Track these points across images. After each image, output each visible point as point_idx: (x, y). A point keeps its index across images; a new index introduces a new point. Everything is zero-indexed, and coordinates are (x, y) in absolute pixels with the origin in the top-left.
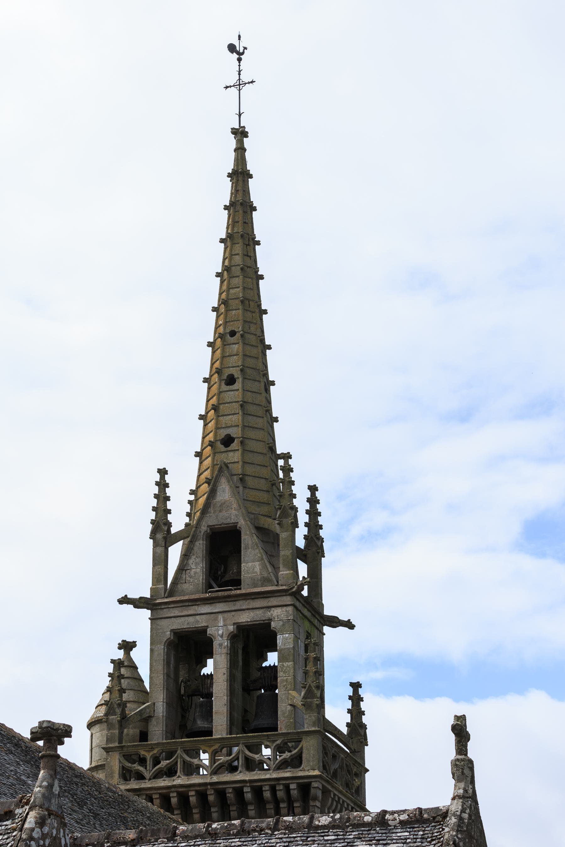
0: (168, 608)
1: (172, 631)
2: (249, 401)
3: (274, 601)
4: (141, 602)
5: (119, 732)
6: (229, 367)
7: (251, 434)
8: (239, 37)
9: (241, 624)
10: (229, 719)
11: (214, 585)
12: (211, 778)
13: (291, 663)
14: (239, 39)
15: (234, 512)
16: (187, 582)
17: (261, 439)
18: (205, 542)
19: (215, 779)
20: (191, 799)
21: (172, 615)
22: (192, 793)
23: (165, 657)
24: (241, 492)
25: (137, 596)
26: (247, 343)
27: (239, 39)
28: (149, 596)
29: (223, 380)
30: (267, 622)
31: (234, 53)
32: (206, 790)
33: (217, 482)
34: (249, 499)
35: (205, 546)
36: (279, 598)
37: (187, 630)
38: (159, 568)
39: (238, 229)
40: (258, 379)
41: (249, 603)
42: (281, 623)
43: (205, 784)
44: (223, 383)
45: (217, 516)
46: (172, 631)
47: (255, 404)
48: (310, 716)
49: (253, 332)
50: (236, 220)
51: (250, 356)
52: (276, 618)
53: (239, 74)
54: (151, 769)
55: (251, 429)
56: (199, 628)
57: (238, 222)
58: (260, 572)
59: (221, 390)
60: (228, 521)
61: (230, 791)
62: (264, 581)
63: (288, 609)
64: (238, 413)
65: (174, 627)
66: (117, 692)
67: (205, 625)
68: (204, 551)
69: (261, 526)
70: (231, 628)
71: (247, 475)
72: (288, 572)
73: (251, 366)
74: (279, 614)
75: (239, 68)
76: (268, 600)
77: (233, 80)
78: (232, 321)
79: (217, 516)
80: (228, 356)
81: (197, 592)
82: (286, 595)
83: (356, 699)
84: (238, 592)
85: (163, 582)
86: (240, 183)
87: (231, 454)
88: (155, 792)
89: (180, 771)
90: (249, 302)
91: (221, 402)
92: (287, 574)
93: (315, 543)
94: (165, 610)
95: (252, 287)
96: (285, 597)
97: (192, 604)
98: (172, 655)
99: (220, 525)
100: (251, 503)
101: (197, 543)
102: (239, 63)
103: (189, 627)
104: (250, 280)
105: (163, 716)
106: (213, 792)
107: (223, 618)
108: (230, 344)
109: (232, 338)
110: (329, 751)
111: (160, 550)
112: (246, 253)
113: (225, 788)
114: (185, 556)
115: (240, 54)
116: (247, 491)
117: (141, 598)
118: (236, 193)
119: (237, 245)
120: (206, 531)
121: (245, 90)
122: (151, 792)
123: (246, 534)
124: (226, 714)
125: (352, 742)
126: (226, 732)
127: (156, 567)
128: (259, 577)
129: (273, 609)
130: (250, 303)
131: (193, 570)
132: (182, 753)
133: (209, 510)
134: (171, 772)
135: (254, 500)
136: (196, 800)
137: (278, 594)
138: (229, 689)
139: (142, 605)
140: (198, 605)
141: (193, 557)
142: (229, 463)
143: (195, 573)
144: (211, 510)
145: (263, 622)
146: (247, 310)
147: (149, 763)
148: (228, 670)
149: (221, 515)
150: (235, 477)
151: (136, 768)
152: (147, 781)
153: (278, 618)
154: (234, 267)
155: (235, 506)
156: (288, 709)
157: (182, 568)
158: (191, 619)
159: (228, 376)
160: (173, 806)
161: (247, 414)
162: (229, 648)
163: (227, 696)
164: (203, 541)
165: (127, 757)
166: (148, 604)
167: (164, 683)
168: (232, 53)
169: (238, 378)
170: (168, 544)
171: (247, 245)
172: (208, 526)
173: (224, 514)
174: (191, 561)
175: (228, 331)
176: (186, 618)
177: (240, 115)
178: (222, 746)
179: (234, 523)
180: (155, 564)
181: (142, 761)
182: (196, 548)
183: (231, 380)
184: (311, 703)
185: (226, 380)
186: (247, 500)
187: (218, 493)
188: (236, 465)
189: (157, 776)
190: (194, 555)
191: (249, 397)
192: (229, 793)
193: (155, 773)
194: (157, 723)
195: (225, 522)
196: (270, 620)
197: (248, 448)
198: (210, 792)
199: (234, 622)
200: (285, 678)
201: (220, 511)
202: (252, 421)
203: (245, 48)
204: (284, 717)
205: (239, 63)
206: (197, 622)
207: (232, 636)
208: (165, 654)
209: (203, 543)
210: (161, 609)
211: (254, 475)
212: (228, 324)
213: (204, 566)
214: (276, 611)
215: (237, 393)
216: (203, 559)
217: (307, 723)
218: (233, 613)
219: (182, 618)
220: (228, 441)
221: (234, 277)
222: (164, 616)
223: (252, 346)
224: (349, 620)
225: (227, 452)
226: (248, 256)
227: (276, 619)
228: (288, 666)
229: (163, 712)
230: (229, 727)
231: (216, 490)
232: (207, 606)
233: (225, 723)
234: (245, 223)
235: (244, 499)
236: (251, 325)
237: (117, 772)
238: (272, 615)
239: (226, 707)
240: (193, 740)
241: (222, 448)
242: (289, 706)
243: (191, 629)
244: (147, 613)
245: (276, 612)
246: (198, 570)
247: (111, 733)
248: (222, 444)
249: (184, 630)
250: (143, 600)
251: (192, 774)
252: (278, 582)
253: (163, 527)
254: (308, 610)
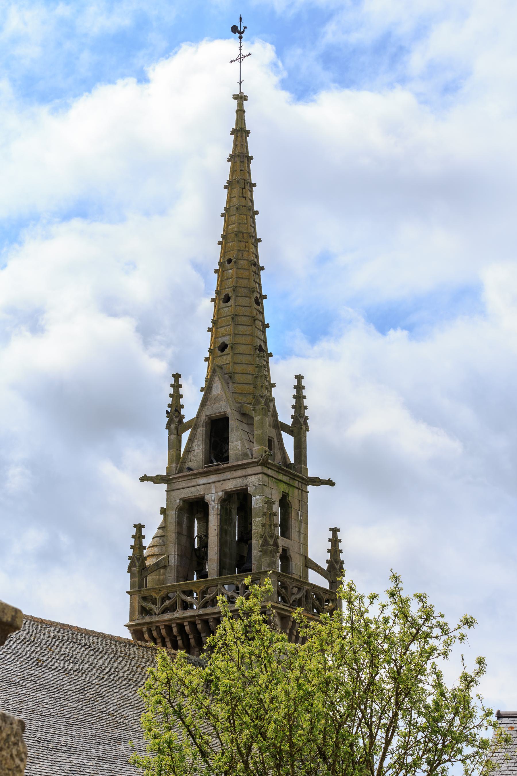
0: (178, 482)
1: (180, 499)
2: (240, 314)
3: (249, 471)
4: (157, 479)
5: (138, 580)
6: (226, 288)
7: (240, 339)
8: (241, 19)
9: (228, 491)
10: (219, 564)
11: (214, 460)
12: (199, 611)
13: (261, 518)
14: (241, 21)
15: (224, 403)
16: (192, 460)
17: (249, 343)
18: (204, 428)
19: (201, 612)
20: (186, 628)
21: (181, 487)
22: (186, 624)
23: (177, 519)
24: (230, 387)
25: (154, 475)
26: (240, 267)
27: (241, 21)
28: (165, 474)
29: (221, 299)
30: (245, 487)
31: (237, 33)
32: (196, 620)
33: (212, 380)
34: (238, 392)
35: (204, 431)
36: (253, 468)
37: (191, 497)
38: (172, 451)
39: (236, 177)
40: (248, 296)
41: (232, 473)
42: (254, 488)
43: (194, 616)
44: (221, 302)
45: (212, 407)
46: (180, 499)
47: (245, 316)
48: (266, 560)
49: (245, 258)
50: (235, 169)
51: (242, 278)
52: (251, 484)
53: (240, 50)
54: (160, 606)
55: (241, 336)
56: (200, 496)
57: (236, 171)
58: (241, 449)
59: (220, 307)
60: (220, 410)
61: (211, 621)
62: (244, 455)
63: (259, 477)
64: (231, 325)
65: (182, 496)
66: (138, 549)
67: (202, 493)
68: (204, 436)
69: (244, 412)
70: (220, 494)
71: (236, 373)
72: (259, 447)
73: (243, 286)
74: (253, 480)
75: (240, 45)
76: (245, 470)
77: (236, 55)
78: (229, 251)
79: (212, 407)
80: (226, 279)
81: (199, 468)
82: (258, 466)
83: (335, 541)
84: (225, 466)
85: (175, 462)
86: (239, 138)
87: (225, 357)
88: (161, 624)
89: (179, 607)
90: (243, 234)
91: (219, 317)
92: (258, 449)
93: (299, 421)
94: (176, 483)
95: (246, 222)
96: (257, 467)
97: (194, 477)
98: (185, 518)
99: (215, 414)
100: (239, 395)
101: (199, 430)
102: (241, 40)
103: (192, 495)
104: (245, 216)
105: (174, 565)
106: (200, 622)
107: (215, 486)
108: (227, 270)
109: (229, 265)
110: (289, 585)
111: (173, 437)
112: (241, 195)
113: (208, 619)
114: (191, 440)
115: (241, 33)
116: (236, 385)
117: (157, 476)
118: (236, 147)
119: (235, 190)
120: (205, 420)
121: (245, 61)
122: (159, 624)
123: (232, 420)
124: (216, 561)
125: (330, 575)
126: (216, 575)
127: (171, 451)
128: (240, 453)
129: (249, 477)
130: (244, 235)
131: (196, 451)
132: (180, 593)
133: (207, 403)
134: (172, 608)
135: (241, 392)
136: (190, 628)
137: (252, 465)
138: (219, 541)
139: (158, 481)
140: (198, 478)
141: (196, 441)
142: (223, 365)
143: (198, 453)
144: (208, 403)
145: (242, 488)
146: (241, 241)
147: (159, 602)
148: (219, 527)
149: (215, 406)
150: (227, 375)
151: (150, 606)
152: (157, 616)
153: (252, 484)
154: (232, 208)
155: (224, 398)
156: (258, 554)
157: (188, 450)
158: (193, 489)
159: (225, 296)
160: (200, 631)
161: (238, 325)
162: (219, 510)
163: (217, 547)
164: (203, 427)
165: (144, 599)
166: (164, 480)
167: (175, 540)
168: (235, 33)
169: (232, 296)
170: (179, 432)
171: (243, 188)
172: (206, 416)
173: (217, 405)
174: (194, 444)
175: (226, 260)
176: (190, 488)
177: (241, 83)
178: (206, 587)
179: (224, 412)
180: (170, 448)
181: (154, 602)
182: (198, 434)
183: (227, 299)
184: (267, 549)
185: (224, 299)
186: (236, 393)
187: (213, 389)
188: (228, 365)
189: (164, 612)
190: (196, 439)
191: (240, 311)
192: (211, 622)
193: (163, 609)
194: (171, 571)
195: (218, 411)
196: (247, 485)
197: (238, 351)
198: (198, 622)
199: (222, 489)
200: (256, 530)
201: (215, 403)
202: (242, 329)
203: (245, 28)
204: (255, 561)
205: (241, 40)
206: (198, 491)
207: (222, 500)
208: (176, 517)
209: (203, 430)
210: (173, 483)
211: (242, 372)
212: (226, 254)
213: (204, 447)
214: (251, 479)
215: (230, 308)
216: (203, 442)
217: (264, 565)
218: (222, 482)
219: (188, 489)
220: (223, 347)
221: (232, 215)
222: (176, 488)
223: (245, 269)
224: (330, 479)
225: (222, 356)
226: (243, 197)
227: (251, 485)
228: (259, 521)
229: (175, 562)
230: (218, 571)
231: (212, 387)
232: (204, 478)
233: (216, 568)
234: (242, 170)
235: (232, 393)
236: (244, 253)
237: (137, 610)
238: (248, 481)
239: (216, 555)
240: (186, 583)
241: (219, 353)
242: (259, 552)
243: (194, 497)
244: (164, 487)
245: (252, 480)
246: (199, 451)
247: (133, 581)
248: (219, 350)
249: (189, 498)
250: (159, 477)
251: (186, 609)
252: (252, 456)
253: (175, 420)
254: (285, 475)
